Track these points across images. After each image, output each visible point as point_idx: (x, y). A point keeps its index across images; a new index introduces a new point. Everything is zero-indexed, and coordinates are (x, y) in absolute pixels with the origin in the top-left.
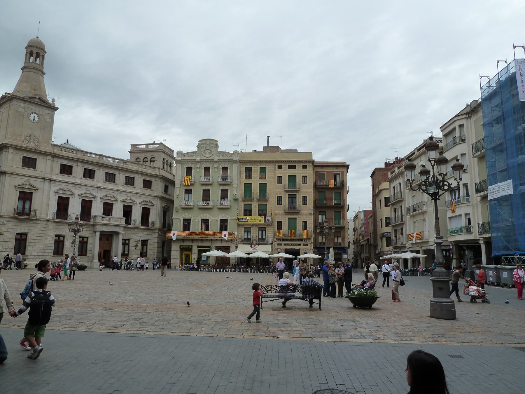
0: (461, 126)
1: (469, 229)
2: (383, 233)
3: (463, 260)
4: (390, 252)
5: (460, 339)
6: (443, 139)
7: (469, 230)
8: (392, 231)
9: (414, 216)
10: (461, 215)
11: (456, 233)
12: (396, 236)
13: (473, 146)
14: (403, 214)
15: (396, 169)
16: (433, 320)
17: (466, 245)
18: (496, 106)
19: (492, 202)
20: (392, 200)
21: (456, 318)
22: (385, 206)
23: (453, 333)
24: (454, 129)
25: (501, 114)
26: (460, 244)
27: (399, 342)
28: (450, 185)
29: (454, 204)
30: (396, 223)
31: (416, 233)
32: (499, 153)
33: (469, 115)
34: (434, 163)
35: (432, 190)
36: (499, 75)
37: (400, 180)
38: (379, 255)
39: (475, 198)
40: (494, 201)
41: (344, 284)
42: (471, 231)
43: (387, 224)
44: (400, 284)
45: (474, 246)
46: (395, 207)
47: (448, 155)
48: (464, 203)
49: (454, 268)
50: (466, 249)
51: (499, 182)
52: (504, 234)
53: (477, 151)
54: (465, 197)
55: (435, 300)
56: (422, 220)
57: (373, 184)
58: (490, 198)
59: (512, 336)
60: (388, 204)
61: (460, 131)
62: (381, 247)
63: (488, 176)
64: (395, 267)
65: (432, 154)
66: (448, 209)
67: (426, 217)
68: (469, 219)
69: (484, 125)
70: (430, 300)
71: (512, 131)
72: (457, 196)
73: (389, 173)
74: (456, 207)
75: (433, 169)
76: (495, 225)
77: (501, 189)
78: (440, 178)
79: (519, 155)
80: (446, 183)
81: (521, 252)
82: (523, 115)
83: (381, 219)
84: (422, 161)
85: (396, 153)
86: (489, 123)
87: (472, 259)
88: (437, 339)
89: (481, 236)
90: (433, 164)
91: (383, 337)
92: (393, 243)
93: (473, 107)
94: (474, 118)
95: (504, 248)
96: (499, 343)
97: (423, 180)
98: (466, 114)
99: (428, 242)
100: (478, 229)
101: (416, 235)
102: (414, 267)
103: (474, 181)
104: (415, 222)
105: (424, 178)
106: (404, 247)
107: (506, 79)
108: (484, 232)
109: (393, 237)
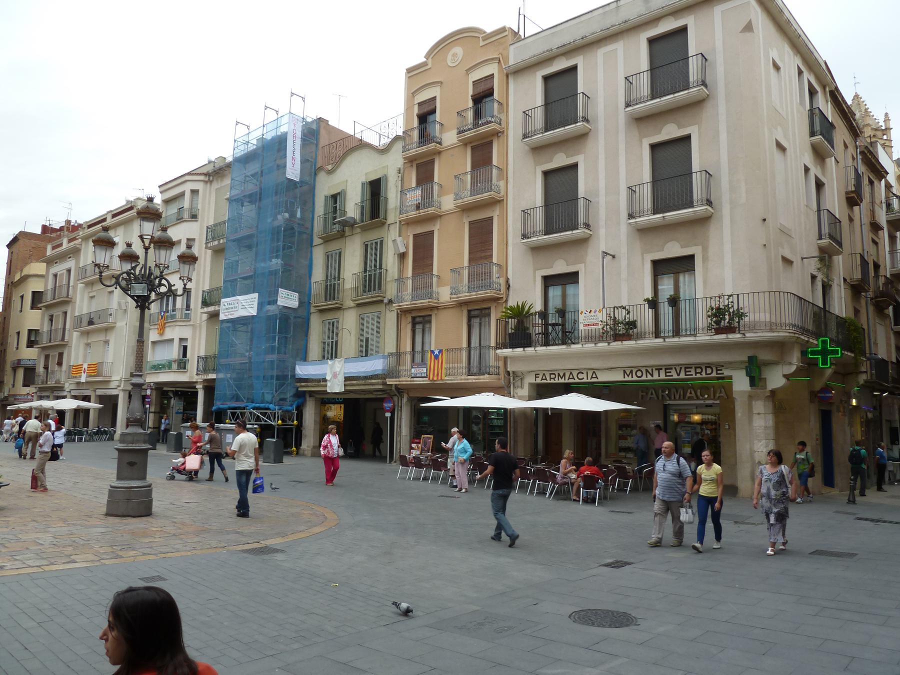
0: (194, 192)
1: (182, 364)
2: (19, 360)
3: (165, 415)
4: (30, 397)
5: (159, 547)
6: (161, 206)
7: (182, 365)
8: (39, 356)
9: (87, 333)
10: (172, 340)
11: (160, 369)
12: (46, 368)
13: (209, 230)
14: (67, 327)
15: (65, 241)
16: (112, 519)
17: (174, 389)
18: (253, 176)
19: (224, 323)
20: (48, 299)
21: (153, 513)
22: (32, 308)
23: (147, 540)
24: (182, 195)
25: (258, 190)
26: (165, 389)
27: (47, 568)
28: (170, 286)
29: (166, 319)
30: (50, 342)
31: (88, 365)
32: (246, 249)
33: (209, 178)
34: (150, 244)
35: (139, 289)
36: (265, 128)
37: (70, 264)
38: (4, 403)
39: (199, 314)
40: (228, 322)
41: (216, 461)
42: (185, 368)
43: (30, 344)
44: (49, 457)
45: (186, 394)
46: (51, 312)
47: (174, 233)
48: (181, 320)
49: (148, 428)
50: (172, 396)
51: (238, 294)
52: (234, 375)
53: (214, 239)
54: (184, 310)
55: (120, 485)
56: (102, 342)
57: (11, 261)
58: (222, 317)
59: (238, 533)
60: (38, 306)
61: (192, 201)
62: (11, 386)
63: (225, 281)
64: (44, 426)
65: (149, 228)
66: (152, 327)
67: (112, 337)
68: (185, 348)
69: (230, 200)
70: (110, 486)
71: (269, 220)
72: (170, 308)
73: (49, 247)
74: (167, 325)
75: (146, 253)
76: (223, 361)
77: (240, 305)
78: (157, 272)
79: (273, 257)
80: (164, 282)
81: (256, 403)
82: (287, 200)
83: (18, 333)
84: (118, 237)
85: (69, 211)
86: (238, 198)
87: (180, 413)
88: (120, 553)
89: (200, 377)
90: (147, 245)
91: (11, 563)
92: (39, 380)
93: (217, 166)
94: (216, 185)
95: (233, 398)
96: (221, 547)
97: (125, 270)
98: (205, 174)
99: (110, 381)
100: (198, 365)
101: (88, 368)
102: (74, 426)
103: (201, 286)
104: (88, 345)
105: (127, 267)
106: (61, 389)
107: (273, 139)
108: (206, 371)
109: (40, 369)
